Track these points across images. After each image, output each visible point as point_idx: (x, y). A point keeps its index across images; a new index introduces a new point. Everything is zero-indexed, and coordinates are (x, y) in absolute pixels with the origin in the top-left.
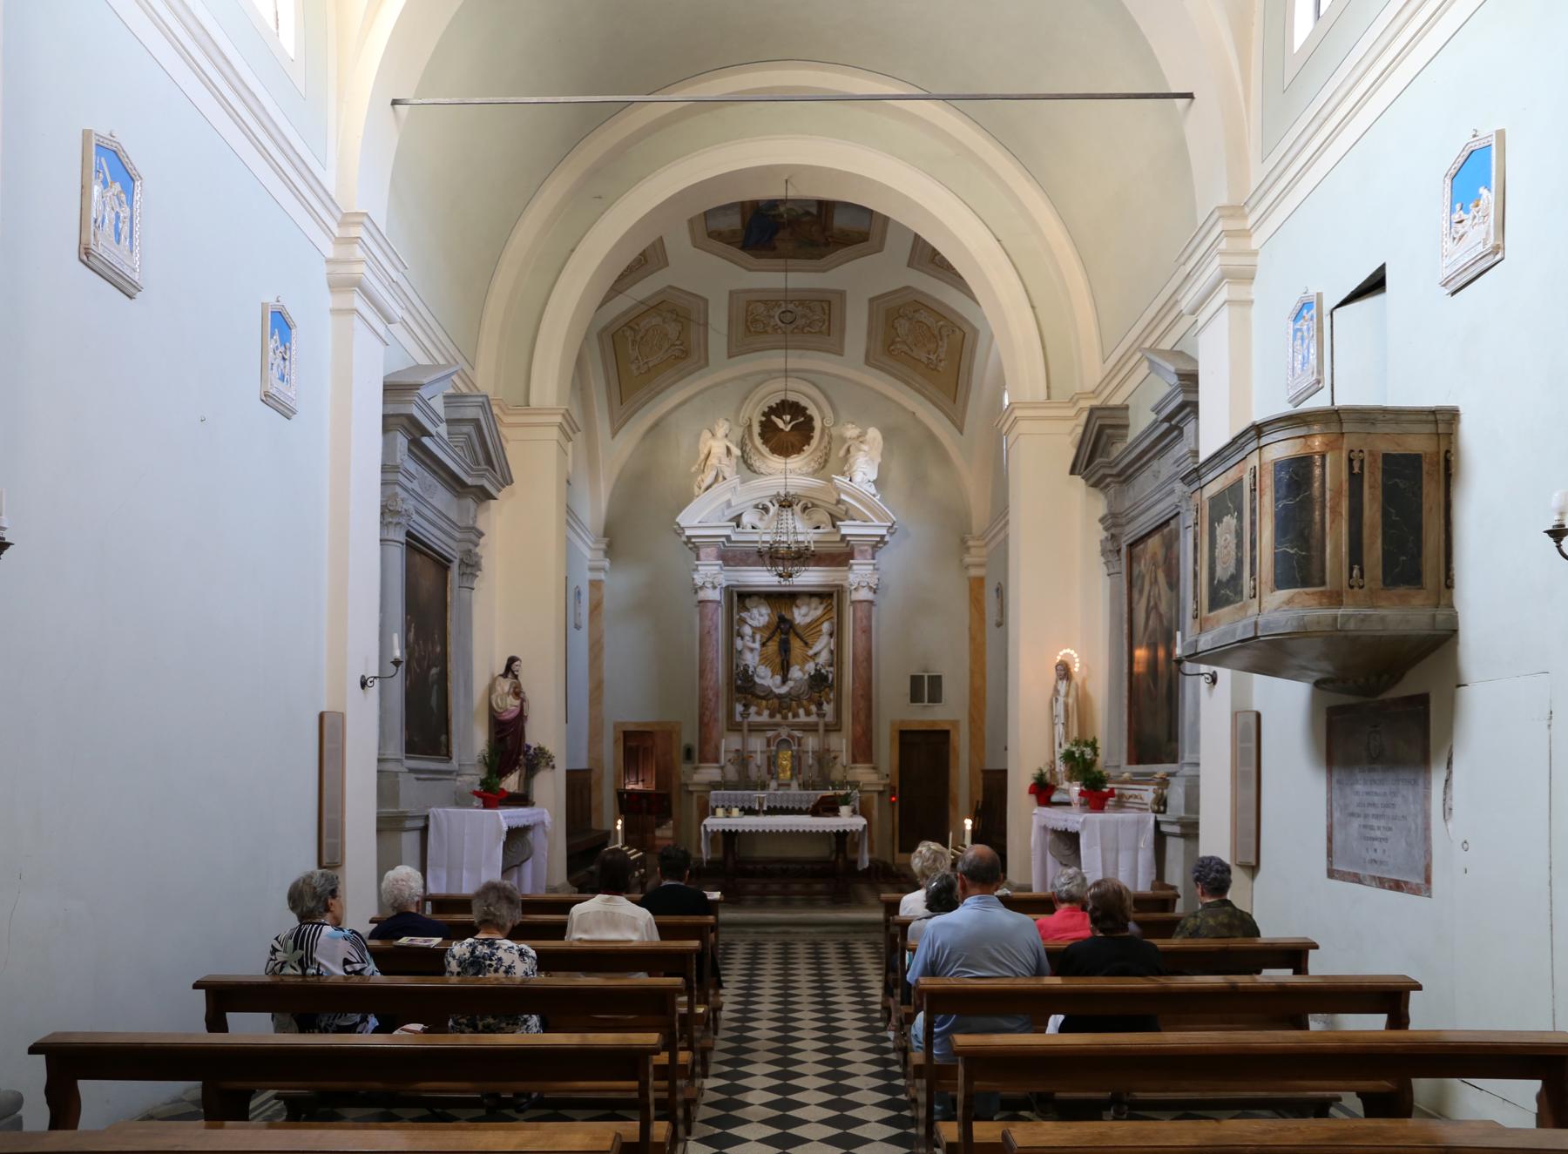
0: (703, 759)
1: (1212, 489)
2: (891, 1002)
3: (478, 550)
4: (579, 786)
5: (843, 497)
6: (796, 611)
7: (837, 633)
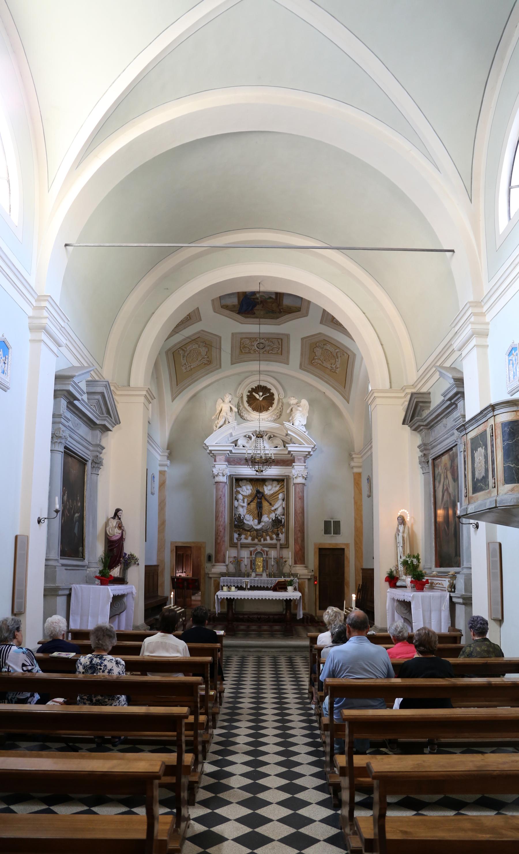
0: (217, 561)
1: (472, 435)
2: (313, 689)
3: (101, 455)
4: (152, 574)
5: (289, 432)
6: (265, 488)
7: (286, 499)
